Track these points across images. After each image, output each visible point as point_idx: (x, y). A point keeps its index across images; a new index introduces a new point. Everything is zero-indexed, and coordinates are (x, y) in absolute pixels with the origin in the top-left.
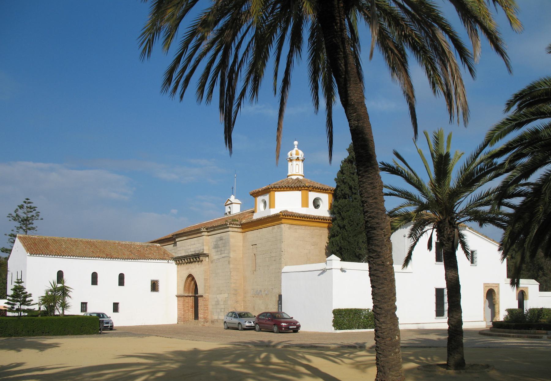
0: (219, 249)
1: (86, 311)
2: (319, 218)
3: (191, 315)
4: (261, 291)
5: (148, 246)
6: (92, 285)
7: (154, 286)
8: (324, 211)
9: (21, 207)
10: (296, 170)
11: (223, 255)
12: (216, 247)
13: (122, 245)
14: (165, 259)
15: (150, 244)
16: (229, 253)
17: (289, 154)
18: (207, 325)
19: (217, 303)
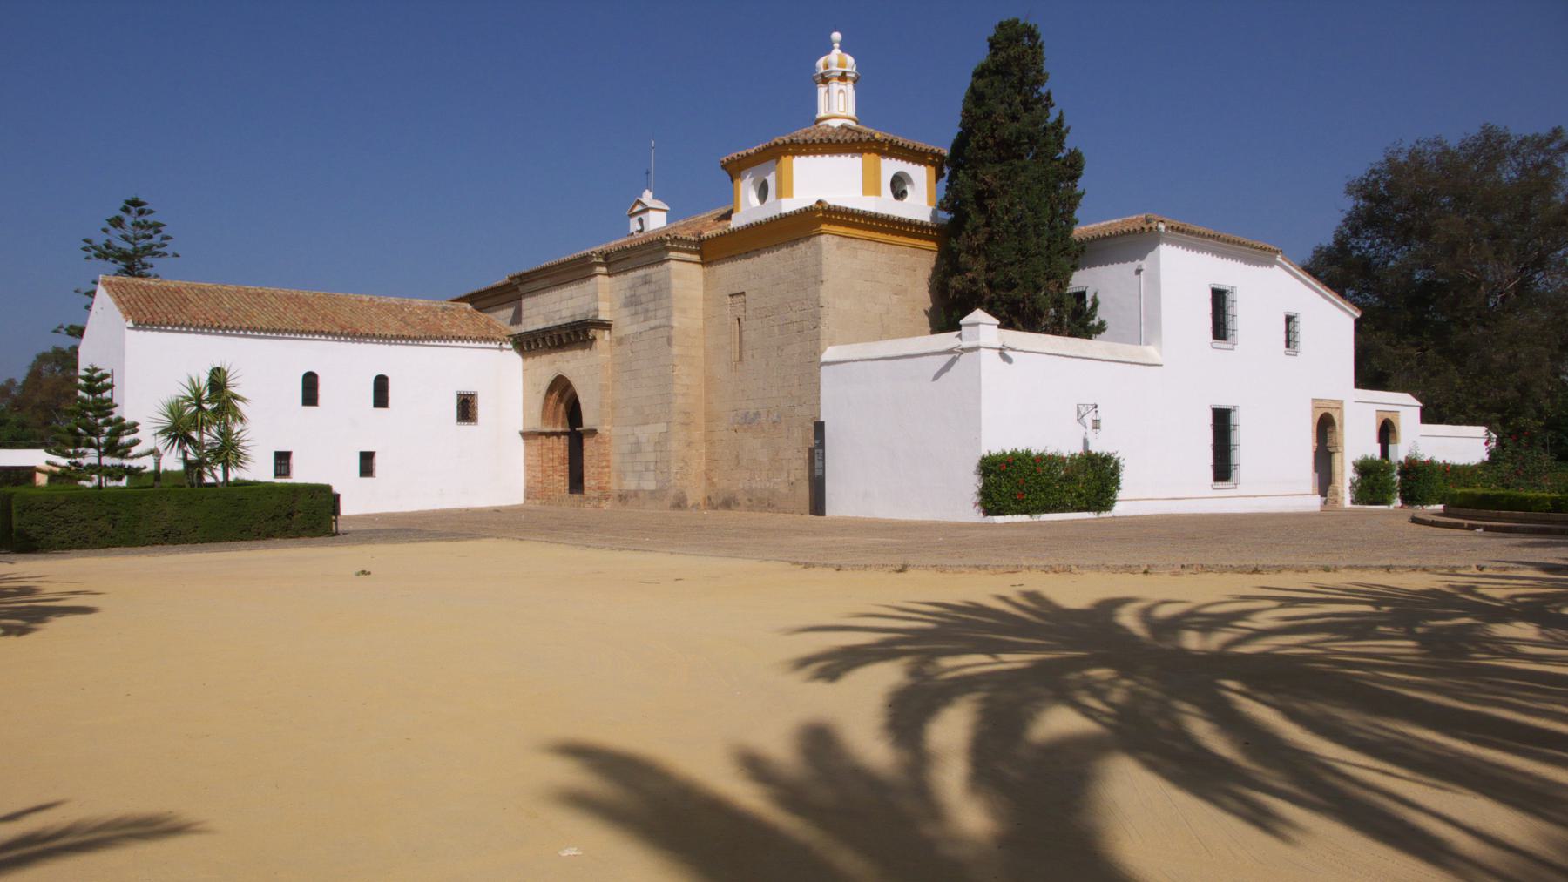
0: (639, 308)
1: (287, 474)
2: (910, 223)
3: (561, 481)
4: (758, 414)
5: (444, 309)
6: (302, 405)
7: (466, 408)
8: (919, 205)
9: (117, 222)
10: (837, 105)
11: (653, 323)
12: (632, 302)
13: (379, 306)
14: (493, 340)
15: (450, 305)
16: (669, 317)
17: (820, 63)
18: (606, 505)
19: (637, 448)
